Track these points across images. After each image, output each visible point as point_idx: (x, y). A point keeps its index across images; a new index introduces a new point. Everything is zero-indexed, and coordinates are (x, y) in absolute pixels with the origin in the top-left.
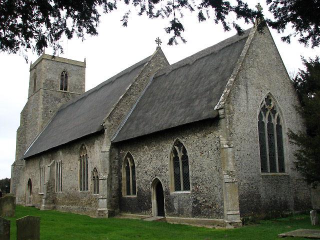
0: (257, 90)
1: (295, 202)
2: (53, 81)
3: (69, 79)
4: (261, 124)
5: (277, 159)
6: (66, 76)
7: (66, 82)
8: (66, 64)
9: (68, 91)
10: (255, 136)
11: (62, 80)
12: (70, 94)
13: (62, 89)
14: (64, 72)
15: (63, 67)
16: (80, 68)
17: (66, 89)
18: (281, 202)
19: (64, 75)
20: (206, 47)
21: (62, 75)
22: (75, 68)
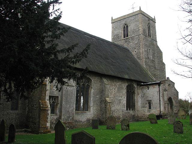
6: (127, 26)
7: (127, 31)
8: (126, 19)
9: (129, 37)
11: (124, 31)
13: (124, 37)
16: (137, 16)
17: (127, 36)
19: (126, 27)
21: (124, 27)
22: (132, 18)
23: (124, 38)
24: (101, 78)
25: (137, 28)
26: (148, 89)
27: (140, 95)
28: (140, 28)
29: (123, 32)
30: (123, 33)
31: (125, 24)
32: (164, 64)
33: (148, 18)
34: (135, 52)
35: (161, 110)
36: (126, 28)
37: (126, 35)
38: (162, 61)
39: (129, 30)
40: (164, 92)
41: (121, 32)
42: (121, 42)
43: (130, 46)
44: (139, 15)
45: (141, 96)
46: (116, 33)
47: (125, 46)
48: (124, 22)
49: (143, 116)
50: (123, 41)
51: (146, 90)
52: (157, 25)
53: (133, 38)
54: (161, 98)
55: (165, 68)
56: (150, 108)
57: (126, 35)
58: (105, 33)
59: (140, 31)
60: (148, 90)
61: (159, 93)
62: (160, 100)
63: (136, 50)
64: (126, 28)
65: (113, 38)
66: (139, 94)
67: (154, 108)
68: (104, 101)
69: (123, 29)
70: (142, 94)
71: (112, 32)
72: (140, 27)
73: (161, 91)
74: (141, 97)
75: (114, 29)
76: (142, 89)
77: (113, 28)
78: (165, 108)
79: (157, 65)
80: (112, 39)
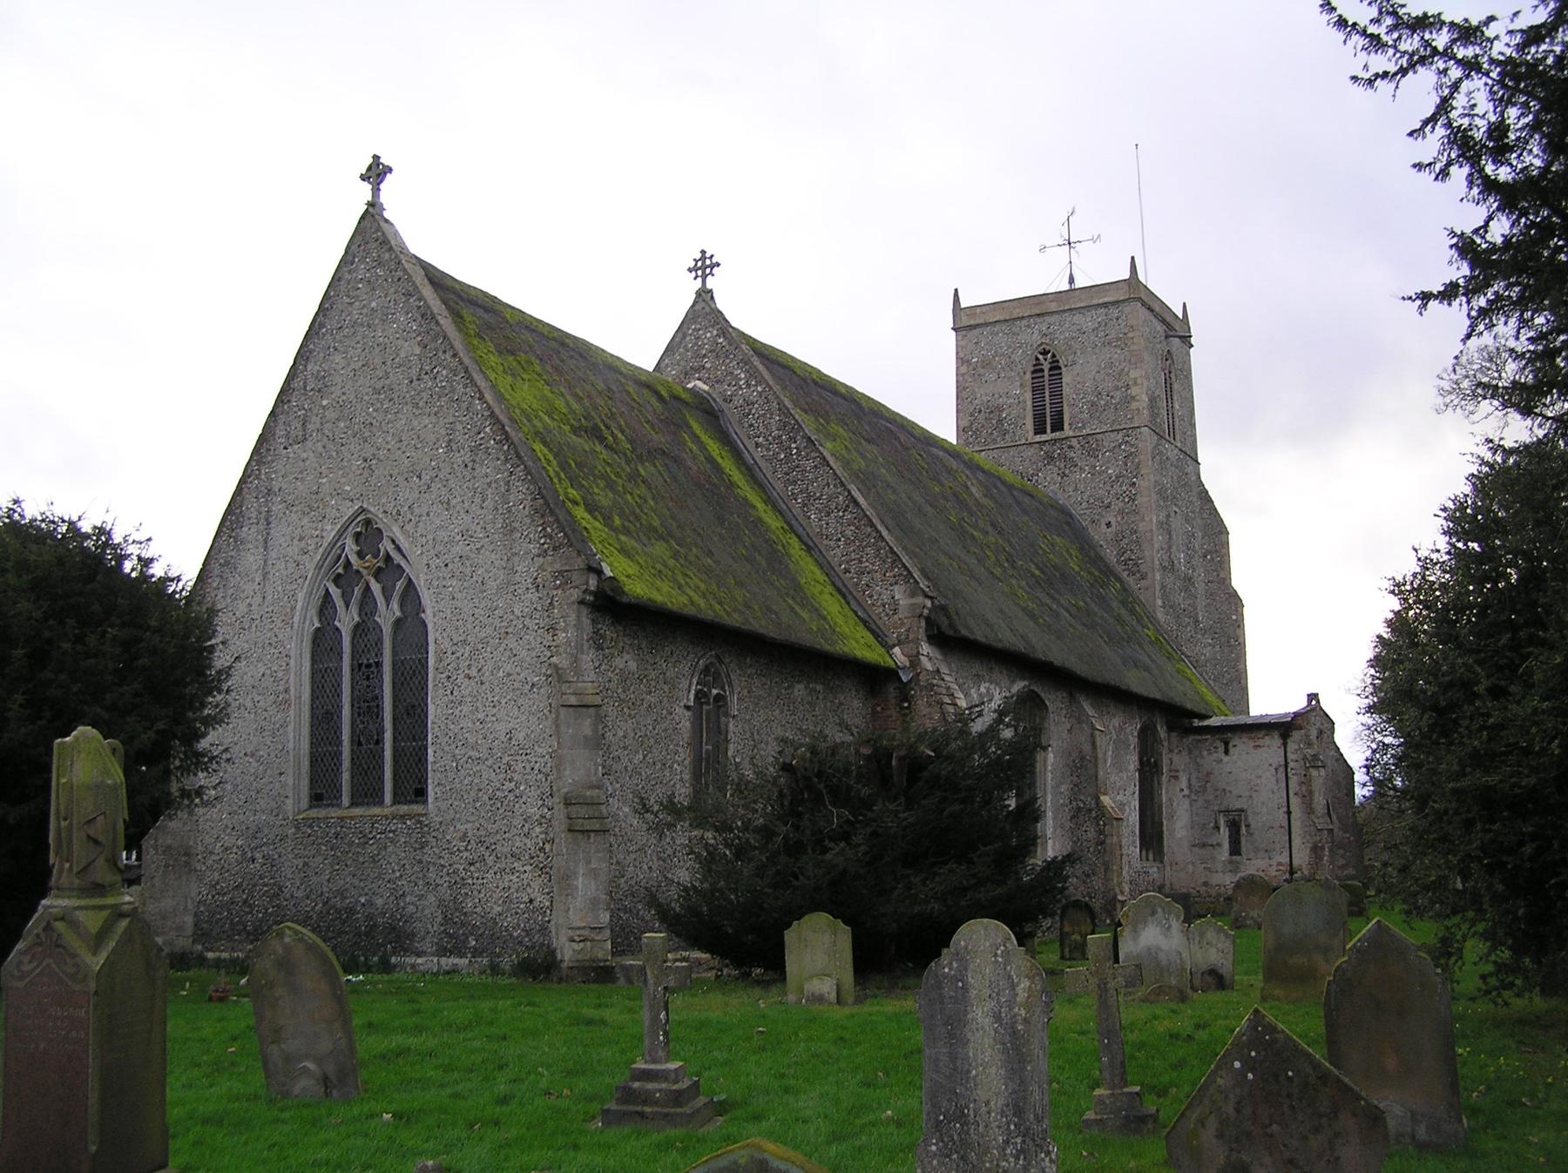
0: (305, 521)
1: (447, 920)
2: (1000, 409)
3: (1067, 378)
4: (323, 642)
5: (388, 754)
6: (1055, 367)
7: (1057, 394)
8: (1048, 319)
9: (1068, 432)
10: (281, 688)
11: (1037, 390)
12: (1074, 442)
13: (1040, 430)
14: (1045, 353)
15: (1032, 337)
16: (1114, 312)
17: (1058, 426)
18: (370, 917)
19: (1046, 367)
20: (546, 320)
21: (1038, 371)
22: (1086, 322)
23: (1038, 438)
24: (1071, 695)
25: (1117, 388)
26: (1226, 752)
27: (1184, 783)
28: (1134, 391)
29: (1028, 395)
30: (1029, 403)
31: (1045, 353)
32: (1235, 601)
33: (1163, 321)
34: (1109, 525)
35: (1296, 862)
36: (1047, 372)
37: (1049, 419)
38: (1225, 581)
39: (1066, 391)
40: (1314, 773)
41: (1017, 396)
42: (1017, 460)
43: (1076, 490)
44: (1127, 309)
45: (1190, 786)
46: (982, 394)
47: (1048, 482)
48: (1036, 338)
49: (1203, 889)
50: (1031, 451)
51: (1212, 758)
52: (1200, 359)
53: (1090, 443)
54: (1294, 801)
55: (1239, 624)
56: (1235, 850)
57: (1049, 419)
58: (921, 388)
59: (1134, 405)
60: (1226, 759)
61: (1282, 776)
62: (1289, 813)
63: (1113, 521)
64: (1047, 372)
65: (964, 423)
66: (1181, 774)
67: (1257, 850)
68: (1090, 810)
69: (1028, 376)
70: (1193, 777)
71: (960, 388)
72: (1136, 383)
73: (1291, 765)
74: (1186, 792)
75: (970, 371)
76: (1196, 752)
77: (961, 361)
78: (1316, 850)
79: (1201, 603)
80: (961, 431)
